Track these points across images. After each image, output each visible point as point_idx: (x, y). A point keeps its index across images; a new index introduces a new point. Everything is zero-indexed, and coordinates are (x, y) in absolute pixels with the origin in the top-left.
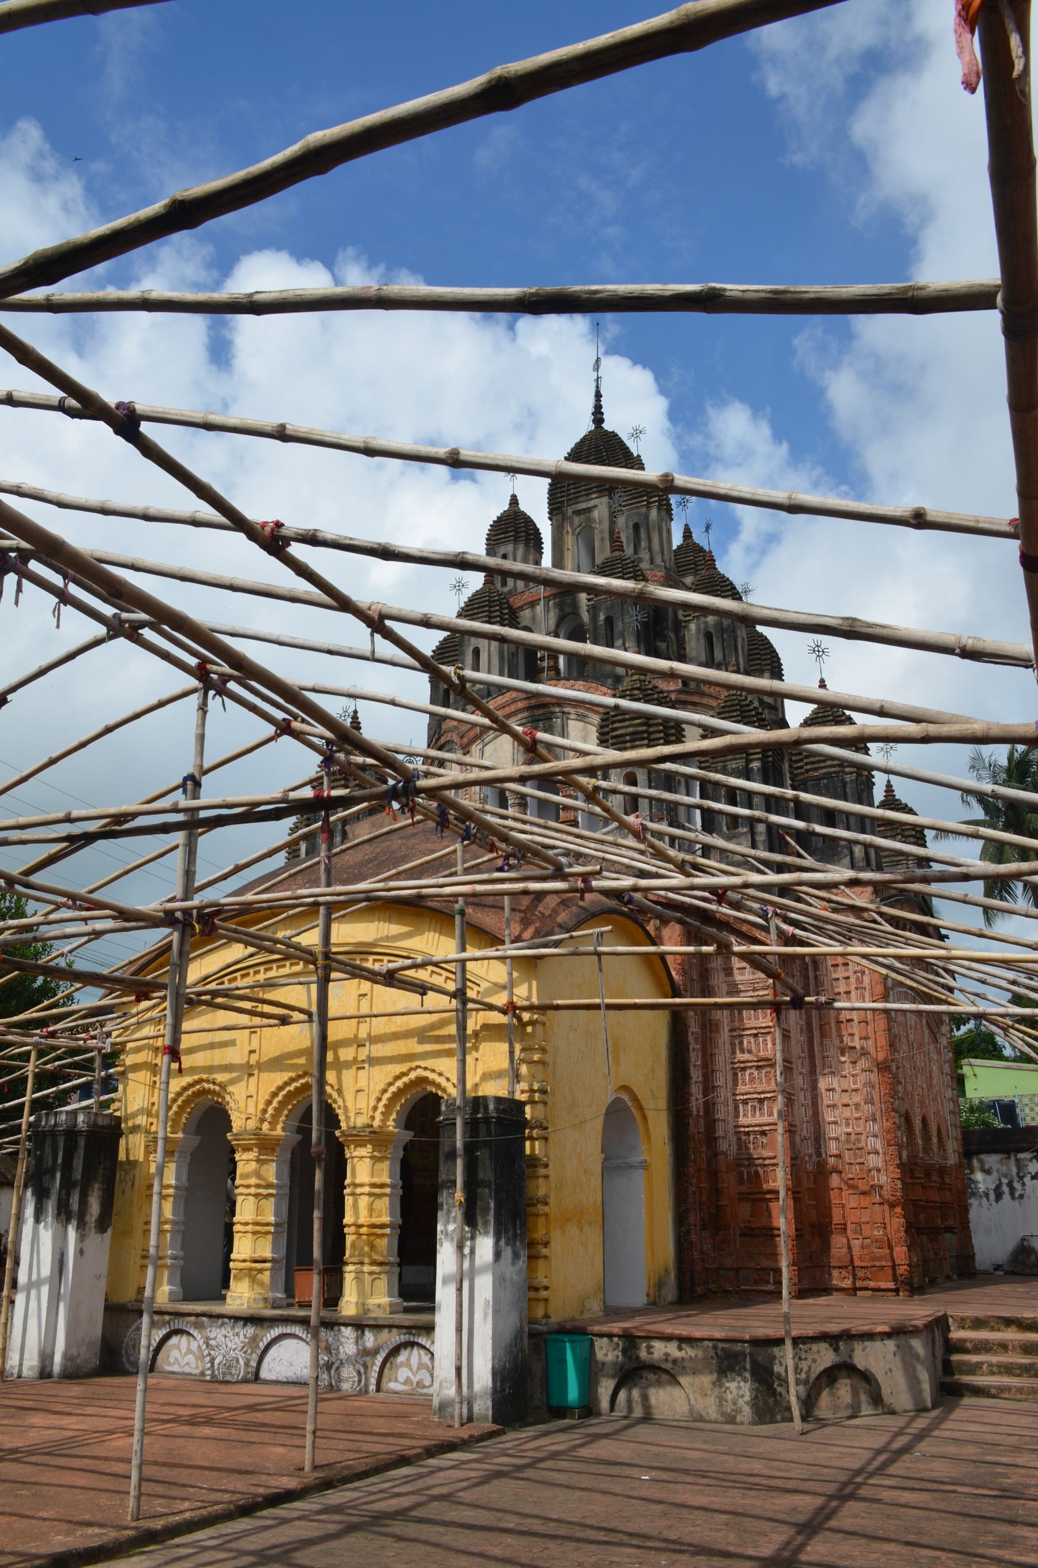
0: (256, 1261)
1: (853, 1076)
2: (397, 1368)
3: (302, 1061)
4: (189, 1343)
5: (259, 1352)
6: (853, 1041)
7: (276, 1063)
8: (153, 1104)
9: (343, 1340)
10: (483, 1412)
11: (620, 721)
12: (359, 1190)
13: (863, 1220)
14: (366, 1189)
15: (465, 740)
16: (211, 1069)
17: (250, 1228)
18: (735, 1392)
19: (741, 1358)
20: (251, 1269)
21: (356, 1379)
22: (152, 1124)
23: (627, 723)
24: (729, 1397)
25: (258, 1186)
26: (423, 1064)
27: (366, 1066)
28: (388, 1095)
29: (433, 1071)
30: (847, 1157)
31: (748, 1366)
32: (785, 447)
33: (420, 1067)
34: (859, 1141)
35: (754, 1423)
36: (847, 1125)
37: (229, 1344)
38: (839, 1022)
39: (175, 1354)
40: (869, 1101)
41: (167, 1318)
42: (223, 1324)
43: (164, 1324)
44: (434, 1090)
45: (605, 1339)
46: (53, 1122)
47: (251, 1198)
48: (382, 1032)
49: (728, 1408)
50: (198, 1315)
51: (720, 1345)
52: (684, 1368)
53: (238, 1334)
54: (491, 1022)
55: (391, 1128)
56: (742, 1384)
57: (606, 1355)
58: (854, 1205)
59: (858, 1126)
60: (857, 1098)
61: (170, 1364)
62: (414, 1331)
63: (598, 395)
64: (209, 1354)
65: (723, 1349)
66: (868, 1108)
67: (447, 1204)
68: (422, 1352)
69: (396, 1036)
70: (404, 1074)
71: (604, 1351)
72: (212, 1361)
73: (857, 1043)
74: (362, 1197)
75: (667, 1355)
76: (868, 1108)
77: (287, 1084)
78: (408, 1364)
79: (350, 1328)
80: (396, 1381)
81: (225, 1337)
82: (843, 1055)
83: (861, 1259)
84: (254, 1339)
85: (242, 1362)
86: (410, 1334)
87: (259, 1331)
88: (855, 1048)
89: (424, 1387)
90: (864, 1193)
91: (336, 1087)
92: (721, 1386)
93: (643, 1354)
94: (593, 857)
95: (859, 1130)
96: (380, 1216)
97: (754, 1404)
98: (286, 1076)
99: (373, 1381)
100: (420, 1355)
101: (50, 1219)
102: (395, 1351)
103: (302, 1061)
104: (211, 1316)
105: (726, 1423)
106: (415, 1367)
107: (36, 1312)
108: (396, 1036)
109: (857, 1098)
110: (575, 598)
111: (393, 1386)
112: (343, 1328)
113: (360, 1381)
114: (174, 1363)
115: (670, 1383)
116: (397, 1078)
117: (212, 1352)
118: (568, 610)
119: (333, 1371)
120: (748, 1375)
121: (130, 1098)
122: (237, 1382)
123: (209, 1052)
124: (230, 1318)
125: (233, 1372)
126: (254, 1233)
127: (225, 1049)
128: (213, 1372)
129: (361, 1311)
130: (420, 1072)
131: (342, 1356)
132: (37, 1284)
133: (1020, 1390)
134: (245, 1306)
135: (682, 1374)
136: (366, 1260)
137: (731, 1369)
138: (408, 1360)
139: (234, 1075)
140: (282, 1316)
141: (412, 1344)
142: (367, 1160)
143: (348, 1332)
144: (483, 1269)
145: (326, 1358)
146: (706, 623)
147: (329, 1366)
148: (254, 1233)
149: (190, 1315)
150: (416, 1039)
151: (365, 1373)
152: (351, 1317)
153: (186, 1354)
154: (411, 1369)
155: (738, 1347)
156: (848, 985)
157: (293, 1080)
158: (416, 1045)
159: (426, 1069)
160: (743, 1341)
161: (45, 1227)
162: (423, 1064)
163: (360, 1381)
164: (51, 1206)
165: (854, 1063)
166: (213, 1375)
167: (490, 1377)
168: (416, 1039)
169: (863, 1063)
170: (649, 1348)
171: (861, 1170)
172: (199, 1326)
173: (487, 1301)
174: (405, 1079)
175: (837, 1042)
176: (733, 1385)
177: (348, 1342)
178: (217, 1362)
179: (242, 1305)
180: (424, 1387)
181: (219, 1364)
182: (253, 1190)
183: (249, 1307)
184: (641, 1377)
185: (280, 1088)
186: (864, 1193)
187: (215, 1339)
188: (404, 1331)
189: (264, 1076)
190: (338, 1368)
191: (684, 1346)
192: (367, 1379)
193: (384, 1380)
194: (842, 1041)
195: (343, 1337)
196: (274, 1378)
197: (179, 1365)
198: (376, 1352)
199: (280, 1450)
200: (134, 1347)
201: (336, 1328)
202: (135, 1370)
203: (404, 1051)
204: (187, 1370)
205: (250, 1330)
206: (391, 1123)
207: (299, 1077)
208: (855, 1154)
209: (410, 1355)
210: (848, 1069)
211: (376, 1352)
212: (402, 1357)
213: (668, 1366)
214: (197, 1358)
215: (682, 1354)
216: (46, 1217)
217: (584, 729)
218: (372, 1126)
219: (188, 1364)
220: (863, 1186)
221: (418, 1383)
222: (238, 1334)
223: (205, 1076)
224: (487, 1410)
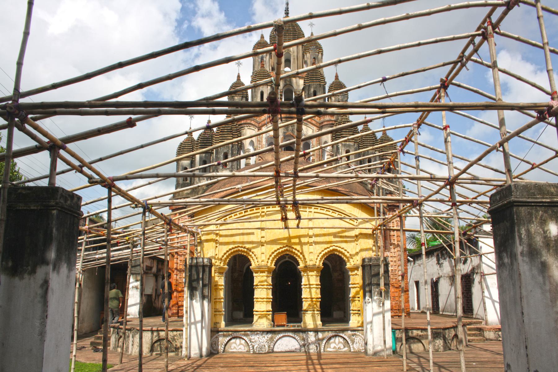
0: (267, 311)
2: (330, 344)
3: (286, 241)
4: (240, 341)
5: (274, 342)
7: (273, 242)
8: (216, 255)
11: (344, 132)
12: (312, 286)
15: (260, 125)
16: (243, 243)
17: (265, 300)
20: (266, 314)
22: (216, 262)
23: (347, 133)
24: (437, 344)
25: (267, 285)
26: (336, 245)
27: (313, 244)
28: (322, 254)
29: (340, 247)
32: (223, 14)
34: (395, 272)
36: (392, 267)
37: (261, 341)
38: (390, 236)
40: (400, 260)
41: (230, 333)
42: (257, 334)
43: (229, 335)
44: (338, 254)
46: (195, 262)
48: (319, 233)
50: (245, 331)
51: (434, 330)
53: (264, 337)
60: (395, 259)
61: (231, 349)
63: (287, 4)
64: (252, 344)
65: (435, 331)
66: (399, 263)
68: (340, 338)
70: (328, 248)
73: (396, 242)
75: (418, 334)
76: (399, 263)
78: (335, 342)
79: (312, 332)
80: (330, 348)
82: (391, 246)
83: (395, 307)
84: (271, 339)
85: (267, 346)
87: (274, 335)
89: (341, 349)
90: (396, 288)
91: (301, 251)
92: (434, 341)
93: (410, 334)
94: (555, 196)
95: (396, 269)
97: (443, 346)
98: (278, 247)
99: (322, 349)
100: (339, 339)
101: (198, 298)
102: (330, 339)
103: (286, 241)
106: (337, 343)
108: (324, 235)
109: (395, 259)
110: (290, 79)
111: (329, 349)
112: (309, 332)
113: (317, 349)
114: (233, 349)
115: (417, 342)
116: (325, 249)
117: (253, 344)
118: (288, 83)
119: (306, 347)
120: (442, 338)
121: (205, 252)
122: (265, 353)
123: (241, 236)
124: (260, 331)
125: (263, 350)
126: (266, 302)
128: (254, 350)
130: (334, 247)
131: (310, 341)
133: (477, 340)
134: (266, 327)
135: (422, 339)
136: (316, 310)
137: (437, 337)
138: (335, 341)
139: (254, 245)
142: (314, 276)
143: (311, 334)
144: (387, 311)
145: (303, 343)
147: (304, 345)
148: (266, 302)
149: (242, 331)
151: (319, 346)
152: (313, 329)
154: (336, 344)
155: (439, 331)
156: (393, 224)
159: (337, 246)
160: (440, 329)
161: (196, 301)
162: (336, 245)
163: (317, 349)
164: (198, 294)
166: (254, 351)
170: (412, 332)
172: (247, 335)
173: (389, 320)
174: (328, 250)
175: (389, 242)
176: (438, 341)
177: (312, 337)
178: (255, 347)
180: (341, 349)
181: (256, 348)
185: (275, 251)
186: (396, 288)
187: (254, 339)
189: (269, 246)
190: (308, 346)
192: (320, 348)
193: (325, 348)
194: (391, 242)
196: (280, 351)
198: (323, 339)
199: (386, 368)
200: (215, 344)
201: (306, 332)
202: (216, 352)
203: (328, 240)
204: (240, 350)
205: (270, 336)
207: (284, 247)
209: (335, 339)
210: (392, 250)
211: (323, 339)
212: (332, 340)
213: (418, 337)
215: (422, 334)
216: (196, 297)
218: (315, 265)
219: (240, 348)
220: (396, 285)
222: (264, 337)
223: (240, 245)
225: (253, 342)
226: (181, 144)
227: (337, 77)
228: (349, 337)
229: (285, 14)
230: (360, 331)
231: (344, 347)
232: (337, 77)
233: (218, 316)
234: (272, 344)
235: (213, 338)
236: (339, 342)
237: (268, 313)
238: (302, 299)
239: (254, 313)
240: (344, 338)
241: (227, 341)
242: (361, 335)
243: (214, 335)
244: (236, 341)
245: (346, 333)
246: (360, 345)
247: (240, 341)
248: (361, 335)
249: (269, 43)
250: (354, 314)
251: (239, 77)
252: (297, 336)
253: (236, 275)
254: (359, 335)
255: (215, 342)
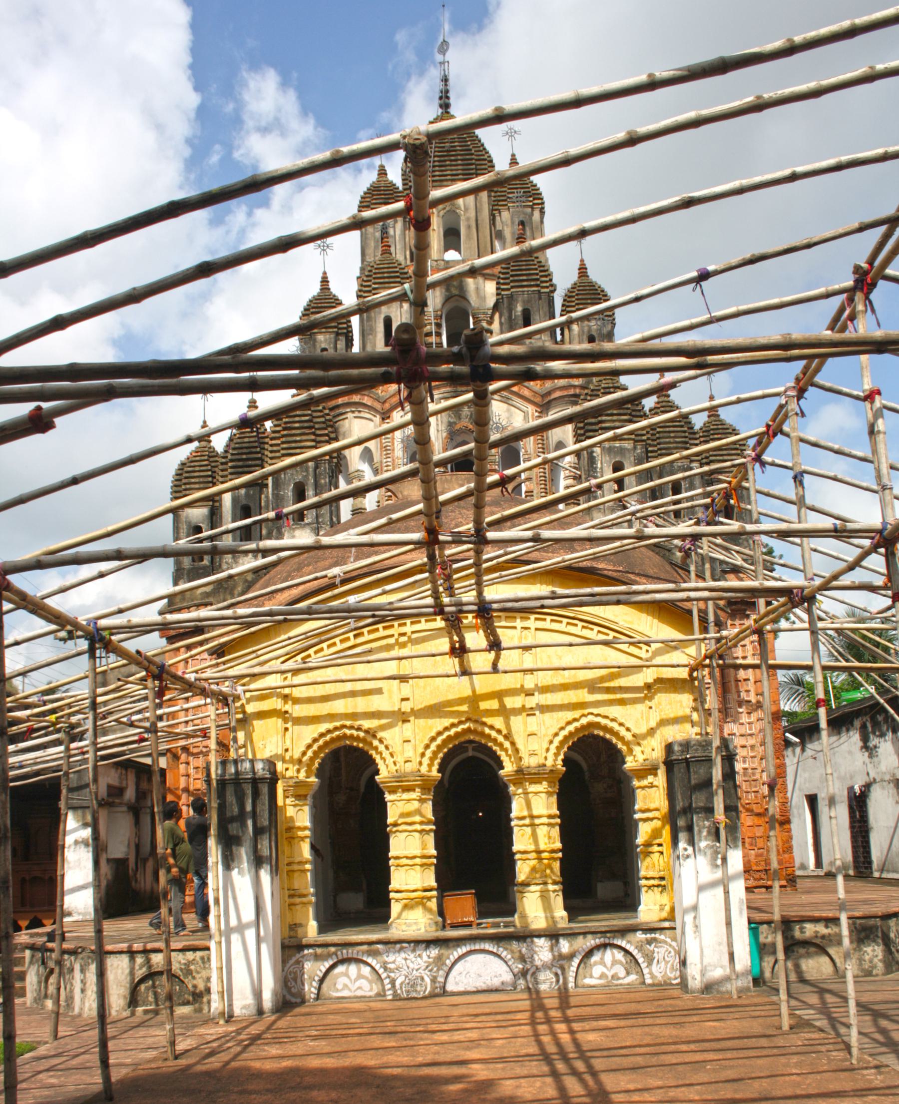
0: (425, 890)
1: (749, 723)
3: (464, 708)
4: (359, 970)
5: (446, 969)
6: (748, 696)
7: (433, 711)
8: (287, 750)
9: (537, 949)
10: (745, 985)
12: (537, 821)
13: (758, 835)
14: (545, 820)
15: (387, 406)
16: (354, 716)
17: (418, 861)
18: (871, 953)
19: (874, 929)
20: (423, 898)
21: (554, 980)
22: (287, 769)
23: (615, 418)
24: (867, 957)
25: (421, 823)
26: (595, 711)
29: (606, 717)
30: (744, 788)
31: (880, 934)
33: (592, 714)
35: (883, 974)
37: (411, 966)
38: (737, 681)
39: (342, 981)
41: (333, 949)
44: (601, 734)
45: (765, 926)
46: (233, 770)
47: (417, 835)
48: (550, 683)
49: (866, 966)
51: (858, 921)
52: (831, 941)
53: (420, 956)
54: (665, 676)
55: (559, 767)
56: (876, 947)
57: (766, 937)
58: (750, 823)
59: (753, 763)
60: (751, 741)
61: (337, 990)
62: (608, 935)
64: (389, 977)
65: (860, 924)
67: (698, 826)
68: (615, 951)
69: (565, 687)
70: (575, 720)
71: (764, 935)
72: (393, 982)
73: (753, 698)
74: (541, 827)
75: (817, 932)
77: (446, 729)
78: (602, 962)
79: (543, 939)
80: (591, 977)
81: (406, 959)
82: (740, 707)
84: (439, 960)
85: (428, 980)
86: (606, 937)
87: (444, 952)
88: (750, 701)
89: (619, 978)
91: (505, 732)
92: (860, 950)
93: (797, 934)
95: (754, 766)
96: (554, 843)
98: (447, 722)
100: (613, 955)
101: (245, 865)
102: (589, 953)
103: (464, 708)
104: (386, 943)
105: (865, 976)
106: (609, 963)
107: (242, 954)
108: (565, 687)
109: (751, 741)
111: (588, 981)
112: (536, 940)
113: (558, 981)
114: (342, 989)
116: (569, 723)
117: (392, 975)
118: (455, 291)
119: (529, 977)
120: (880, 941)
121: (258, 744)
123: (350, 699)
124: (409, 942)
125: (419, 988)
126: (422, 865)
127: (370, 697)
128: (395, 991)
129: (551, 922)
130: (591, 718)
131: (538, 963)
132: (241, 928)
134: (423, 930)
135: (830, 946)
137: (867, 937)
140: (471, 935)
141: (604, 946)
142: (543, 795)
144: (735, 877)
145: (520, 966)
146: (590, 327)
147: (524, 973)
148: (422, 865)
149: (361, 944)
150: (586, 690)
151: (563, 974)
152: (544, 930)
153: (356, 980)
154: (605, 966)
155: (872, 922)
156: (744, 651)
157: (453, 725)
158: (586, 695)
159: (598, 715)
160: (875, 917)
161: (239, 873)
162: (595, 711)
163: (558, 981)
165: (749, 713)
166: (395, 994)
167: (748, 957)
168: (586, 690)
169: (760, 714)
170: (802, 930)
171: (756, 797)
172: (375, 954)
173: (741, 901)
175: (736, 697)
176: (869, 949)
177: (543, 951)
179: (420, 929)
180: (619, 978)
181: (401, 984)
182: (418, 827)
183: (426, 931)
184: (793, 951)
185: (439, 733)
187: (394, 962)
188: (599, 935)
190: (534, 973)
191: (830, 925)
193: (579, 978)
194: (739, 696)
195: (537, 946)
197: (350, 990)
198: (571, 956)
205: (434, 952)
206: (560, 762)
207: (461, 723)
208: (750, 785)
209: (603, 955)
210: (744, 719)
211: (571, 956)
212: (596, 958)
213: (818, 941)
214: (370, 982)
216: (240, 862)
217: (508, 410)
219: (360, 988)
220: (757, 809)
221: (613, 977)
222: (420, 956)
223: (348, 723)
224: (749, 982)
225: (392, 971)
226: (183, 464)
227: (583, 270)
228: (640, 948)
229: (441, 106)
230: (667, 932)
231: (628, 973)
232: (583, 270)
233: (298, 907)
234: (441, 972)
235: (288, 965)
236: (615, 962)
237: (428, 894)
238: (514, 854)
239: (392, 895)
240: (627, 952)
241: (324, 970)
242: (668, 940)
243: (290, 957)
244: (347, 969)
245: (630, 937)
246: (669, 965)
247: (359, 970)
248: (668, 940)
249: (401, 188)
250: (649, 887)
251: (325, 281)
252: (506, 949)
253: (341, 798)
254: (665, 942)
255: (295, 973)
